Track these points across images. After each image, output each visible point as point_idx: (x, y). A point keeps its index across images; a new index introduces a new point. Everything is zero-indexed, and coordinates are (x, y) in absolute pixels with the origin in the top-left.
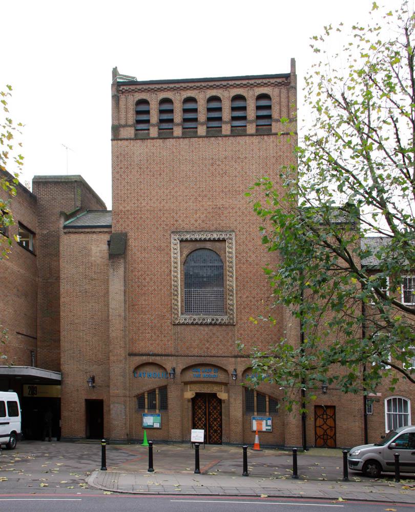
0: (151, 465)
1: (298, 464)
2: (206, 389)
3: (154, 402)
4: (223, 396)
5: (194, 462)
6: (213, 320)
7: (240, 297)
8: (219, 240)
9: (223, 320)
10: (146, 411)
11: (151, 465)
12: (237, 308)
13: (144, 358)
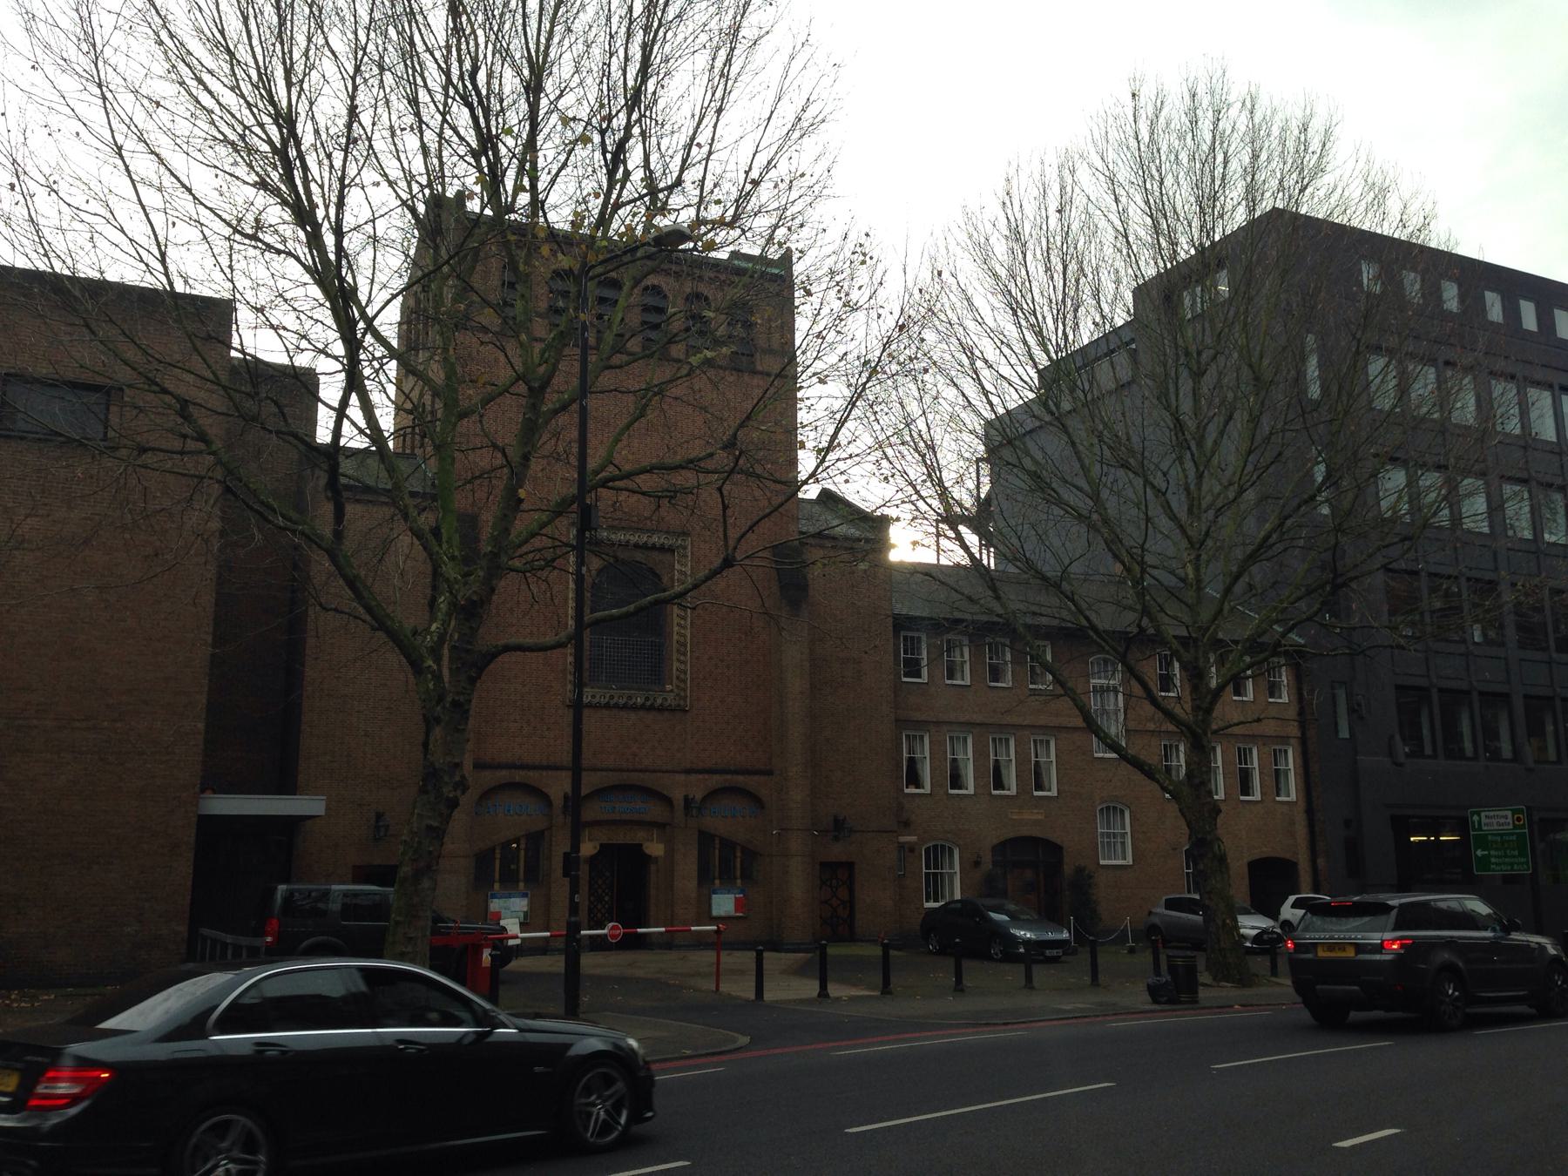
0: (886, 981)
1: (881, 976)
2: (622, 837)
3: (513, 867)
4: (655, 849)
5: (754, 984)
6: (647, 699)
7: (698, 658)
8: (662, 549)
9: (666, 700)
10: (497, 886)
11: (886, 981)
12: (692, 680)
13: (504, 772)
